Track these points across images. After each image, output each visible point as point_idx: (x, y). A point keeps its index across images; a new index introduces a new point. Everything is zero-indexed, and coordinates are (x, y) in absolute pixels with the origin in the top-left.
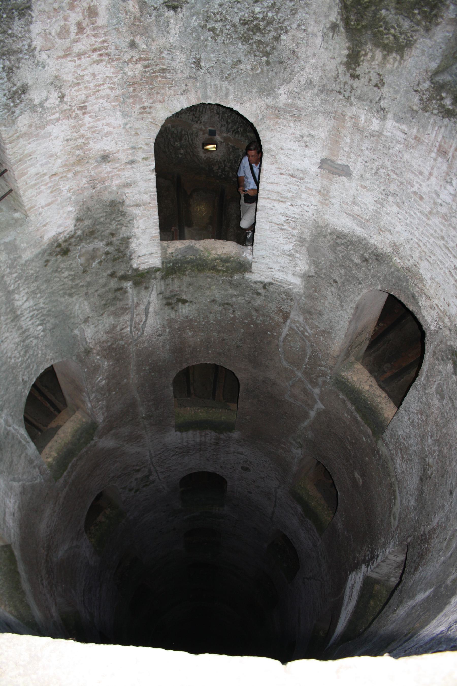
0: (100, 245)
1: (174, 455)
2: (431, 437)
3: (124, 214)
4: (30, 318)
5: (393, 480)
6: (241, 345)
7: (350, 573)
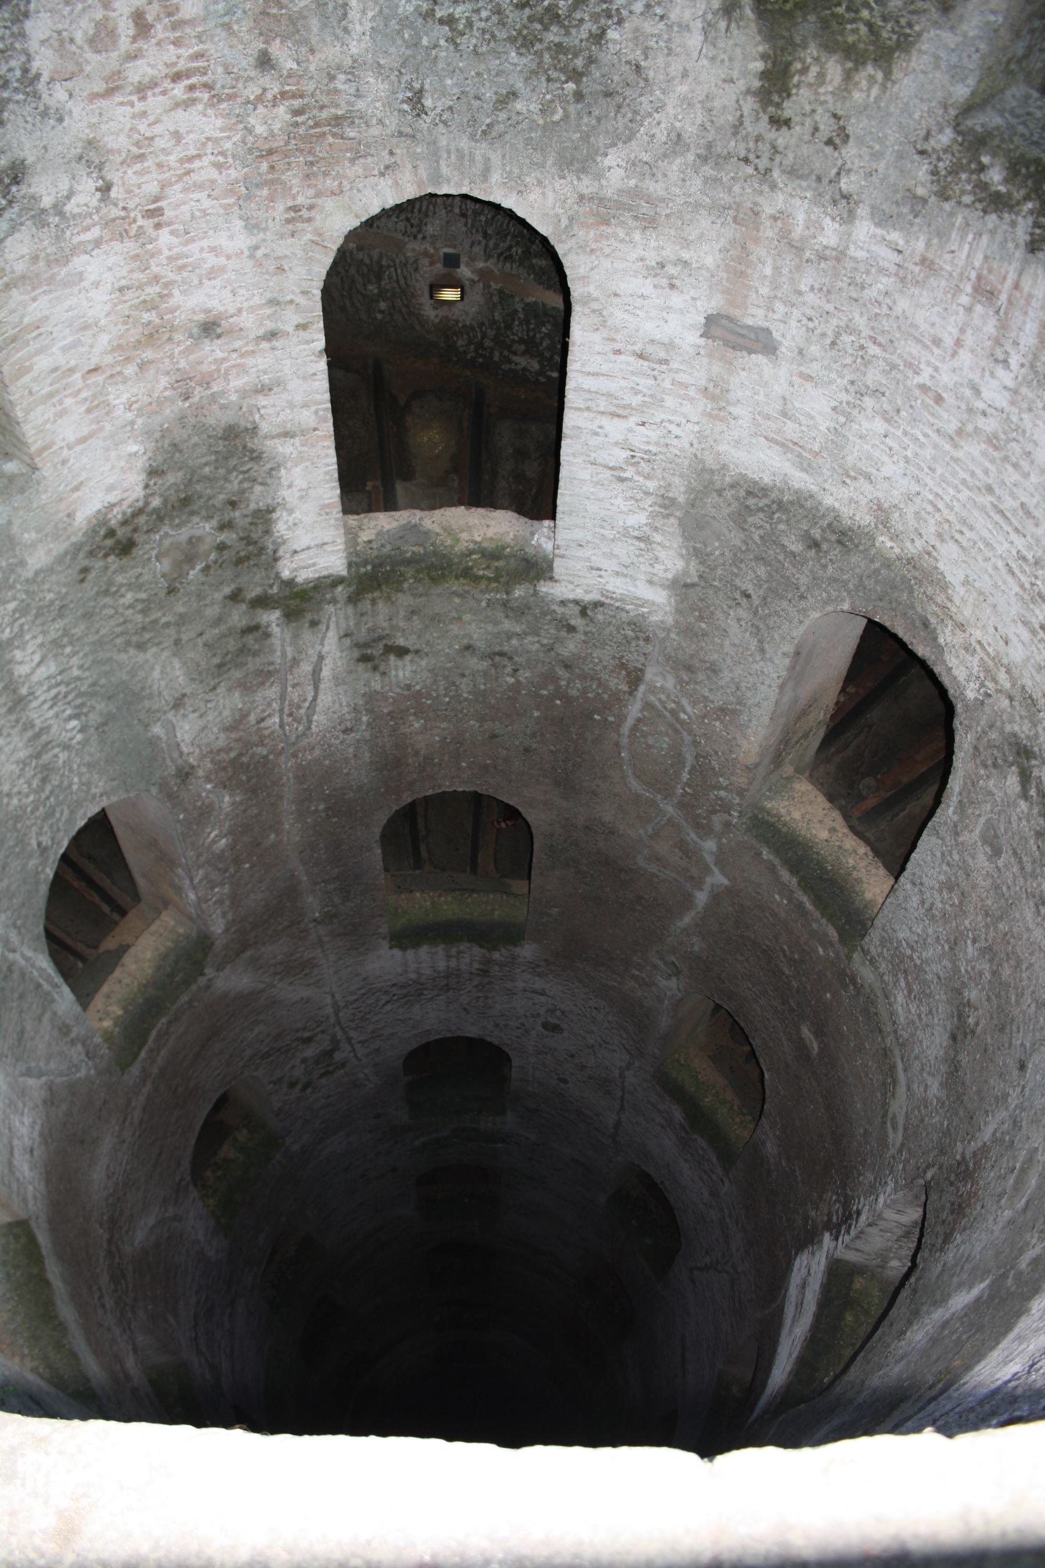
2: (974, 941)
3: (256, 457)
4: (50, 703)
5: (888, 1042)
6: (534, 746)
7: (796, 1254)
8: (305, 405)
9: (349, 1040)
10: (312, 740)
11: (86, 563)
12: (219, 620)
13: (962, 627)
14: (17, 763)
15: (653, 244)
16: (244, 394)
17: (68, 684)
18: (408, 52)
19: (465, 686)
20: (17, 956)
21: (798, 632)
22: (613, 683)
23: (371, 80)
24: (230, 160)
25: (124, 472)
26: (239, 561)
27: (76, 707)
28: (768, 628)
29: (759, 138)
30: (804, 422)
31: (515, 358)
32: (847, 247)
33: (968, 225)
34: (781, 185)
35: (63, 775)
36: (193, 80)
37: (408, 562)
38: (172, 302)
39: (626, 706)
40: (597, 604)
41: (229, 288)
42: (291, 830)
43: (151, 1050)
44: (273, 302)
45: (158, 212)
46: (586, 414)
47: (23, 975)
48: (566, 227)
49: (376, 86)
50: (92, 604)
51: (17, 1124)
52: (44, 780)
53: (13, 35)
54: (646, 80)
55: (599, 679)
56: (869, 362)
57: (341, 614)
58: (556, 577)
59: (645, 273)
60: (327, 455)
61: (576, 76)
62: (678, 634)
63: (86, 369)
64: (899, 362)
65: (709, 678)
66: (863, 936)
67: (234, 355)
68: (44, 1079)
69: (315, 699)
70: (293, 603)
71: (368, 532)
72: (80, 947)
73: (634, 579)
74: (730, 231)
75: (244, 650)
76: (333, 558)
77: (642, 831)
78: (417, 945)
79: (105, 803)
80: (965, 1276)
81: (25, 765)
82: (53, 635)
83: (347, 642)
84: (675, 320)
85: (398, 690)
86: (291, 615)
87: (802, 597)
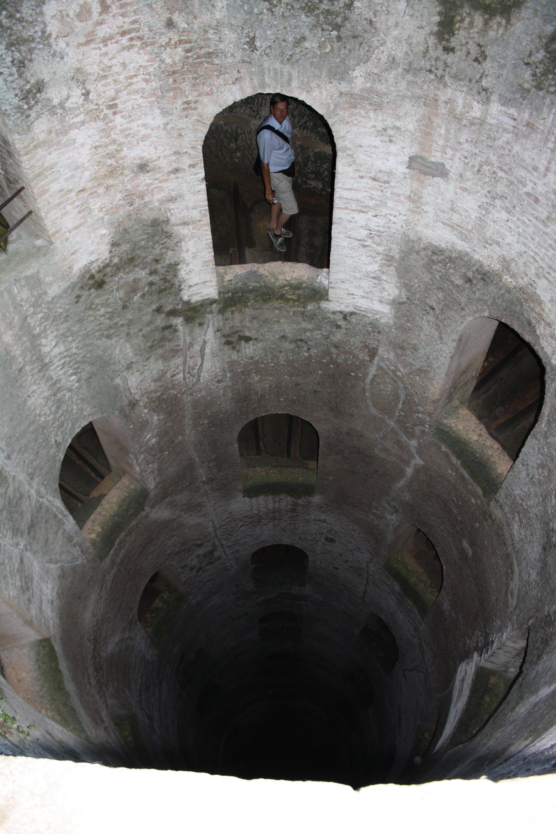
0: (142, 274)
1: (242, 526)
3: (169, 236)
6: (319, 389)
7: (459, 664)
8: (194, 208)
9: (222, 545)
10: (200, 386)
11: (79, 293)
12: (150, 323)
13: (549, 325)
14: (44, 398)
15: (380, 118)
16: (162, 202)
17: (70, 357)
18: (247, 17)
19: (282, 358)
20: (45, 500)
21: (460, 328)
22: (361, 356)
23: (227, 32)
24: (153, 77)
25: (99, 245)
26: (160, 291)
27: (75, 369)
28: (444, 326)
29: (437, 59)
30: (463, 214)
31: (309, 182)
32: (486, 118)
33: (552, 103)
34: (450, 84)
35: (68, 405)
36: (132, 35)
37: (251, 291)
38: (123, 154)
39: (368, 368)
40: (352, 314)
41: (153, 146)
42: (189, 434)
43: (116, 550)
44: (177, 153)
45: (115, 106)
46: (345, 211)
47: (47, 510)
48: (333, 110)
49: (230, 36)
50: (82, 314)
51: (44, 588)
52: (58, 408)
53: (37, 14)
54: (375, 28)
55: (353, 354)
56: (499, 181)
57: (215, 319)
58: (330, 299)
59: (376, 134)
60: (206, 235)
61: (337, 27)
62: (396, 329)
63: (78, 190)
64: (515, 180)
65: (412, 353)
66: (496, 493)
67: (156, 182)
68: (59, 565)
69: (202, 364)
70: (189, 313)
71: (229, 275)
72: (80, 495)
73: (372, 300)
74: (422, 111)
75: (163, 339)
76: (211, 289)
77: (377, 436)
78: (257, 495)
79: (91, 419)
80: (547, 679)
81: (48, 399)
82: (62, 331)
83: (219, 334)
84: (393, 160)
85: (246, 360)
86: (189, 320)
87: (463, 309)
